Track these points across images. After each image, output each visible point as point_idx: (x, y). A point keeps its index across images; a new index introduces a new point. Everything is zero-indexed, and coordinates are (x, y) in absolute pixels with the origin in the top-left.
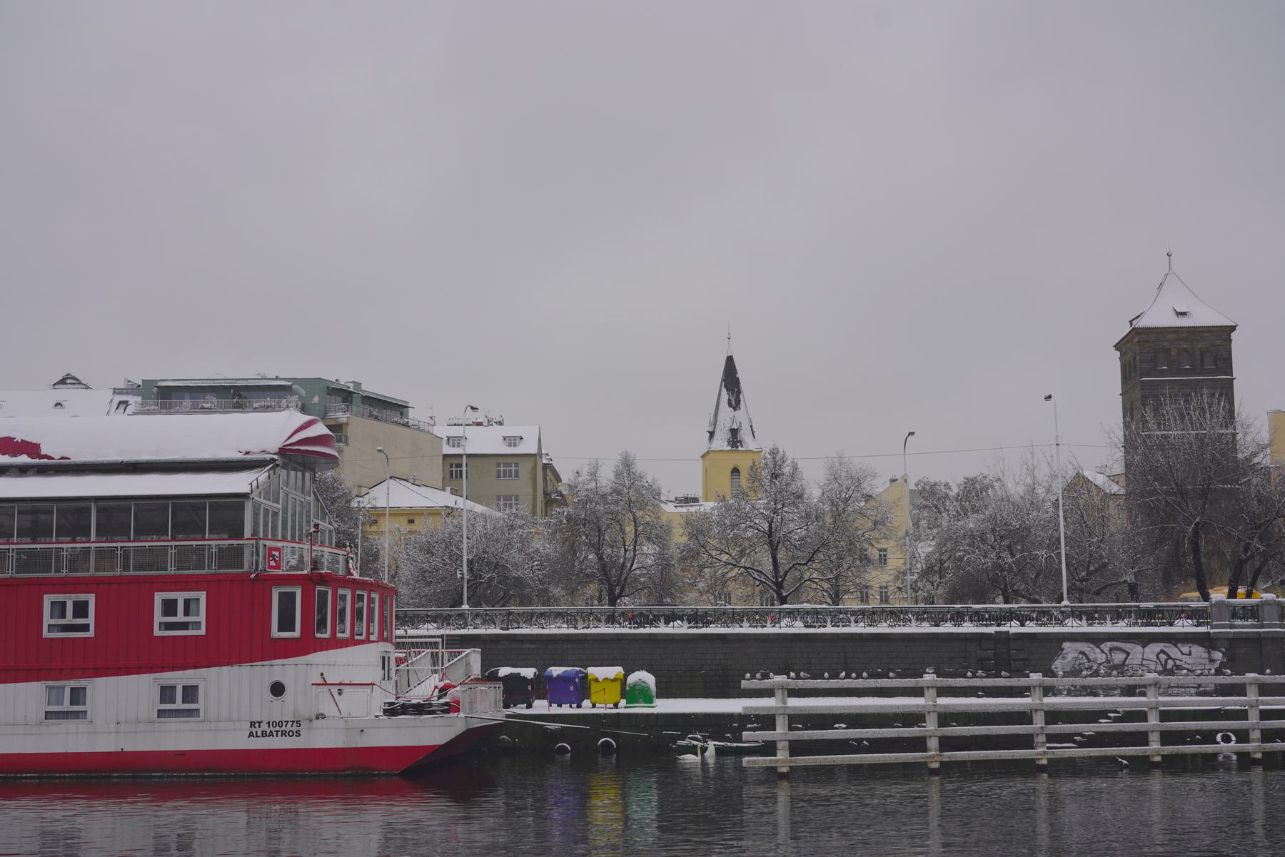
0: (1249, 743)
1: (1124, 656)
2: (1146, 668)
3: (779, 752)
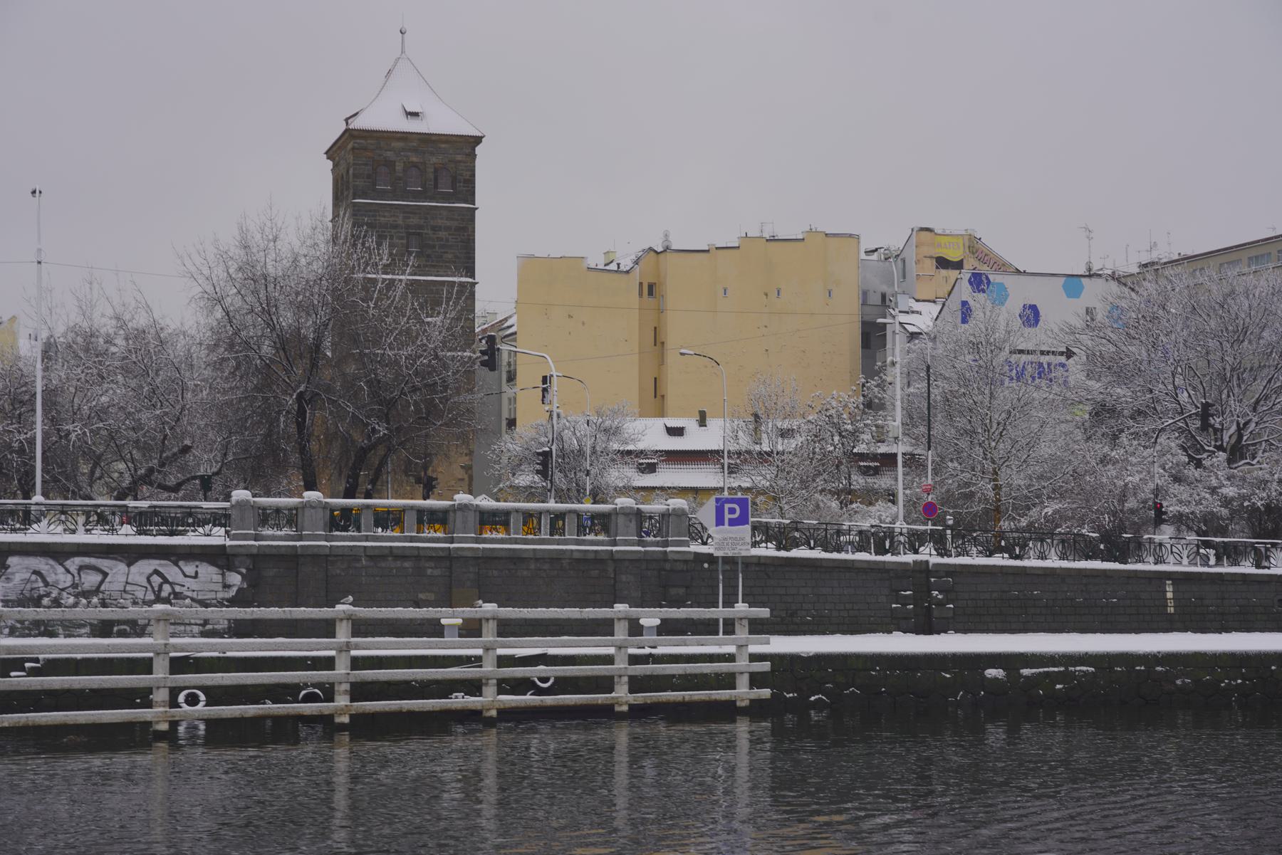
0: (151, 708)
1: (99, 578)
2: (131, 596)
3: (337, 697)
